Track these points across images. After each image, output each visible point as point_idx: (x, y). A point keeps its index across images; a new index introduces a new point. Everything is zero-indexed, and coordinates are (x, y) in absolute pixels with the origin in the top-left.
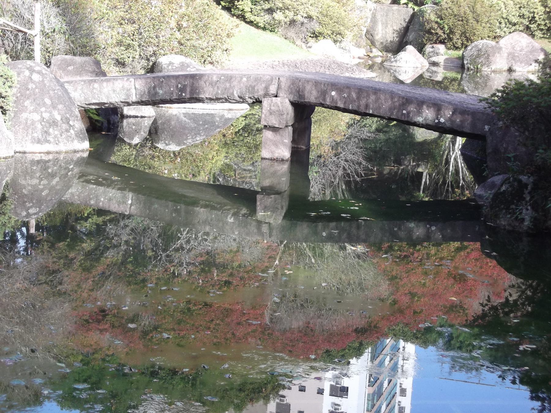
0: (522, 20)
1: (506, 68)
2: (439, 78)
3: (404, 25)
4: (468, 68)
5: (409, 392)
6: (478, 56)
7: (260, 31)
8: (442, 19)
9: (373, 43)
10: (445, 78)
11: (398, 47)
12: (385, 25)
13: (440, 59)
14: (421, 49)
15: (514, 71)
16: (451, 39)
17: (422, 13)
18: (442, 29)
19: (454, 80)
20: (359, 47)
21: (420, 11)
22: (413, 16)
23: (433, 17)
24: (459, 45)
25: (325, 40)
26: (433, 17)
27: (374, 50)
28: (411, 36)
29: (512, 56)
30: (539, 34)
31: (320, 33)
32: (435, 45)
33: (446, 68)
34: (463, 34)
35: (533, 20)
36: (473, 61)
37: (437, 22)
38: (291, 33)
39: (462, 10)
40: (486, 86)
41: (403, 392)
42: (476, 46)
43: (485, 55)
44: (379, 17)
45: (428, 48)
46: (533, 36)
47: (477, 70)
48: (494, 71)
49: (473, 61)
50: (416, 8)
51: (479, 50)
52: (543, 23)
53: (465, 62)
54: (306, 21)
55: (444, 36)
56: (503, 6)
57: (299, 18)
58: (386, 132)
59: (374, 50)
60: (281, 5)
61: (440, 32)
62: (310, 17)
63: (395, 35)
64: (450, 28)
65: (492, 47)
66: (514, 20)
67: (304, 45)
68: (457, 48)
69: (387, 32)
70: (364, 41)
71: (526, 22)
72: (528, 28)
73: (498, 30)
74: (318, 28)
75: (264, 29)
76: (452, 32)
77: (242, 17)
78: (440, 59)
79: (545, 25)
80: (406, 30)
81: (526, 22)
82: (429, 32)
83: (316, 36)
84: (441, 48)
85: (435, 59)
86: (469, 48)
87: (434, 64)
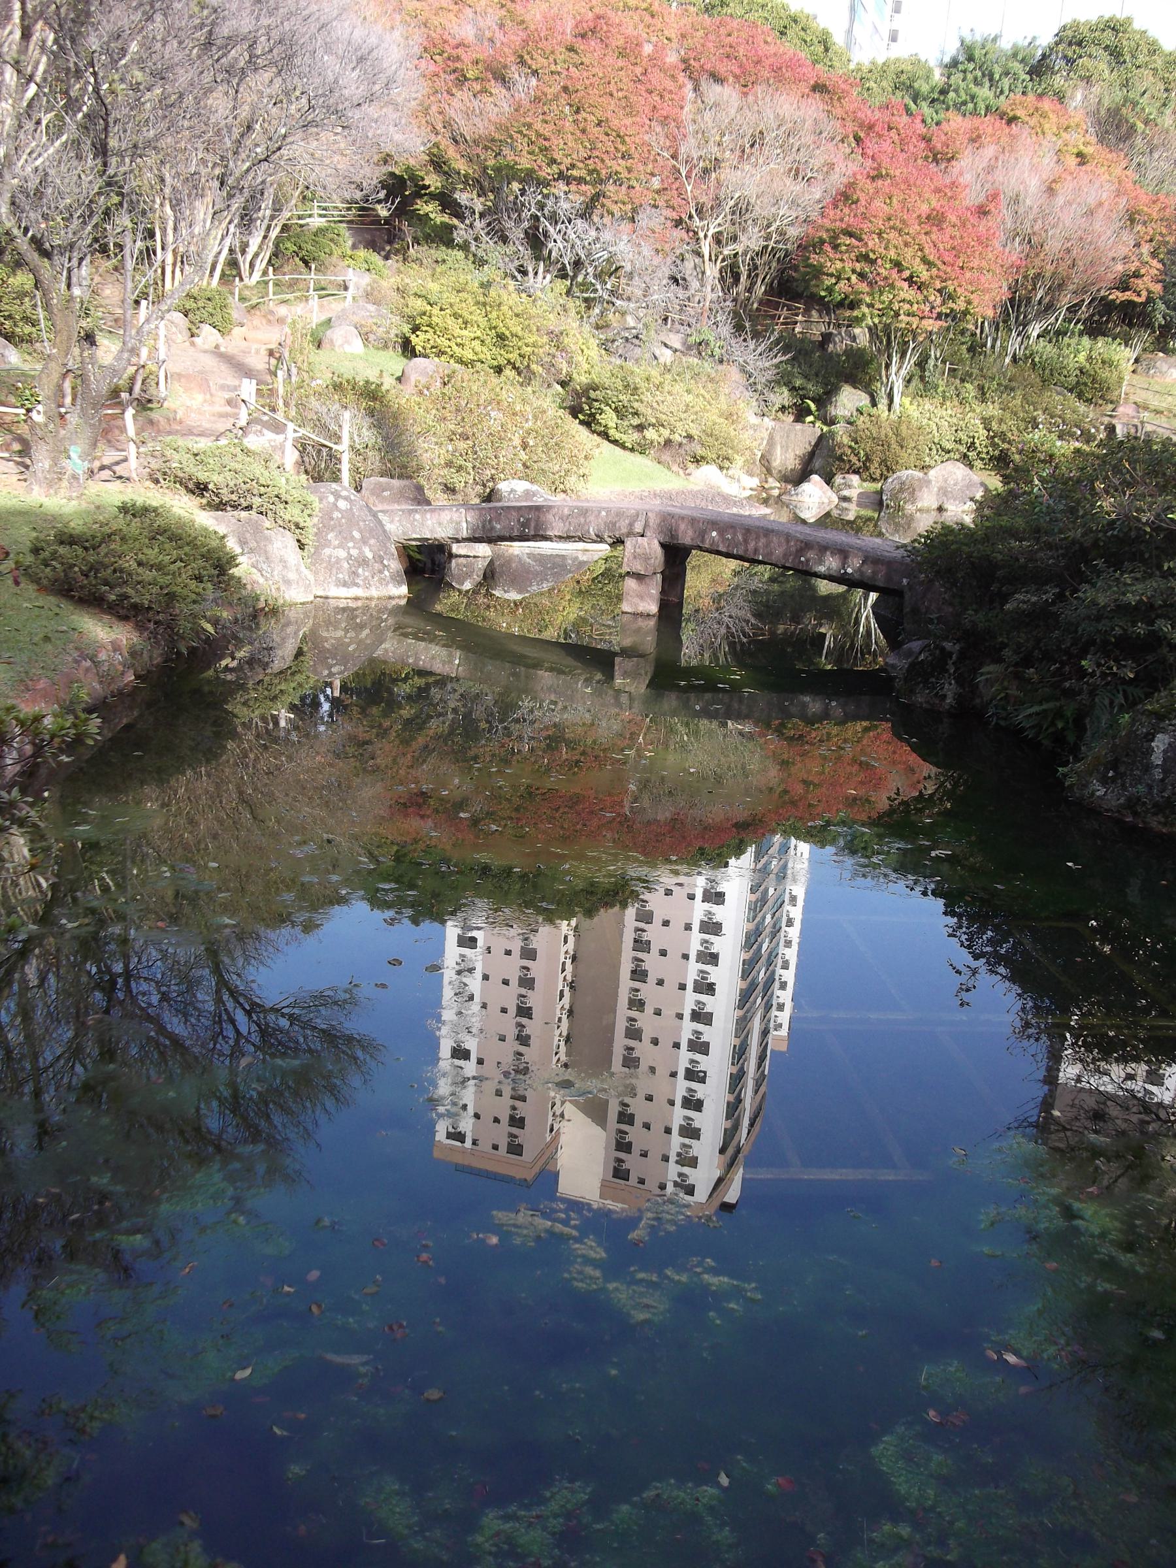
0: (958, 446)
1: (935, 506)
2: (851, 516)
3: (810, 449)
4: (888, 506)
5: (800, 902)
6: (901, 490)
7: (628, 453)
8: (856, 443)
9: (769, 471)
10: (858, 517)
11: (799, 477)
12: (785, 449)
13: (853, 493)
14: (829, 481)
15: (946, 510)
16: (867, 469)
17: (832, 434)
18: (856, 455)
19: (870, 519)
20: (751, 475)
21: (830, 431)
22: (821, 438)
23: (846, 440)
24: (878, 476)
25: (708, 466)
26: (846, 440)
27: (770, 480)
28: (817, 463)
29: (944, 492)
30: (978, 464)
31: (702, 457)
32: (847, 476)
33: (859, 505)
34: (883, 462)
35: (972, 446)
36: (894, 497)
37: (850, 447)
38: (666, 456)
39: (883, 432)
40: (909, 527)
41: (788, 944)
42: (899, 477)
43: (909, 490)
44: (777, 438)
45: (838, 479)
46: (971, 466)
47: (899, 508)
48: (920, 510)
49: (894, 497)
50: (825, 429)
51: (903, 483)
52: (985, 450)
53: (884, 498)
54: (684, 441)
55: (858, 464)
56: (935, 428)
57: (677, 438)
58: (782, 582)
59: (770, 480)
60: (654, 421)
61: (854, 459)
62: (690, 437)
63: (797, 462)
64: (866, 455)
65: (919, 480)
66: (949, 446)
67: (681, 472)
68: (874, 480)
69: (787, 457)
70: (758, 469)
71: (963, 449)
72: (965, 456)
73: (927, 459)
74: (700, 451)
75: (632, 450)
76: (868, 458)
77: (605, 435)
78: (853, 493)
79: (988, 453)
80: (812, 455)
81: (963, 449)
82: (840, 459)
83: (697, 460)
84: (855, 479)
85: (846, 493)
86: (890, 480)
87: (845, 499)
